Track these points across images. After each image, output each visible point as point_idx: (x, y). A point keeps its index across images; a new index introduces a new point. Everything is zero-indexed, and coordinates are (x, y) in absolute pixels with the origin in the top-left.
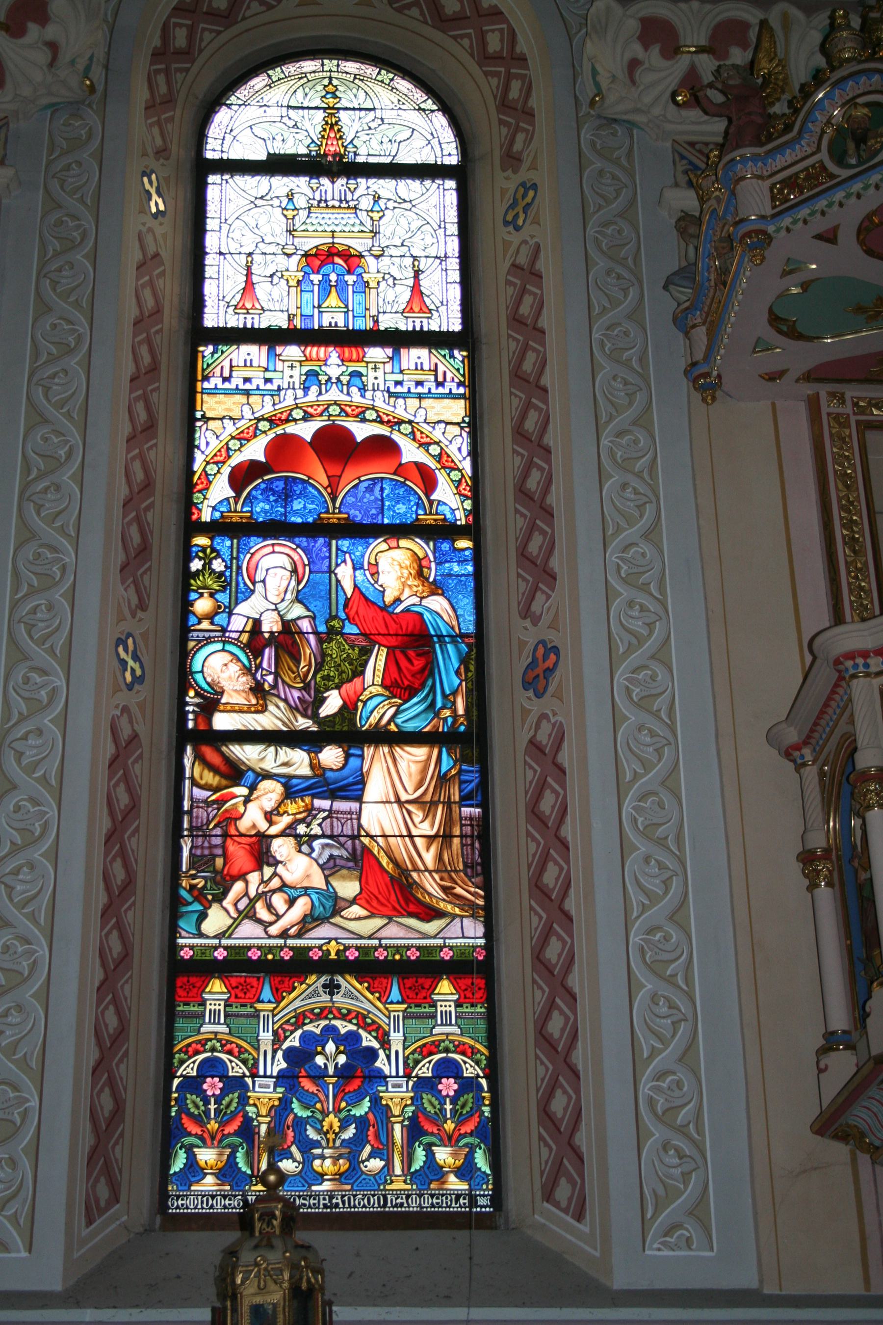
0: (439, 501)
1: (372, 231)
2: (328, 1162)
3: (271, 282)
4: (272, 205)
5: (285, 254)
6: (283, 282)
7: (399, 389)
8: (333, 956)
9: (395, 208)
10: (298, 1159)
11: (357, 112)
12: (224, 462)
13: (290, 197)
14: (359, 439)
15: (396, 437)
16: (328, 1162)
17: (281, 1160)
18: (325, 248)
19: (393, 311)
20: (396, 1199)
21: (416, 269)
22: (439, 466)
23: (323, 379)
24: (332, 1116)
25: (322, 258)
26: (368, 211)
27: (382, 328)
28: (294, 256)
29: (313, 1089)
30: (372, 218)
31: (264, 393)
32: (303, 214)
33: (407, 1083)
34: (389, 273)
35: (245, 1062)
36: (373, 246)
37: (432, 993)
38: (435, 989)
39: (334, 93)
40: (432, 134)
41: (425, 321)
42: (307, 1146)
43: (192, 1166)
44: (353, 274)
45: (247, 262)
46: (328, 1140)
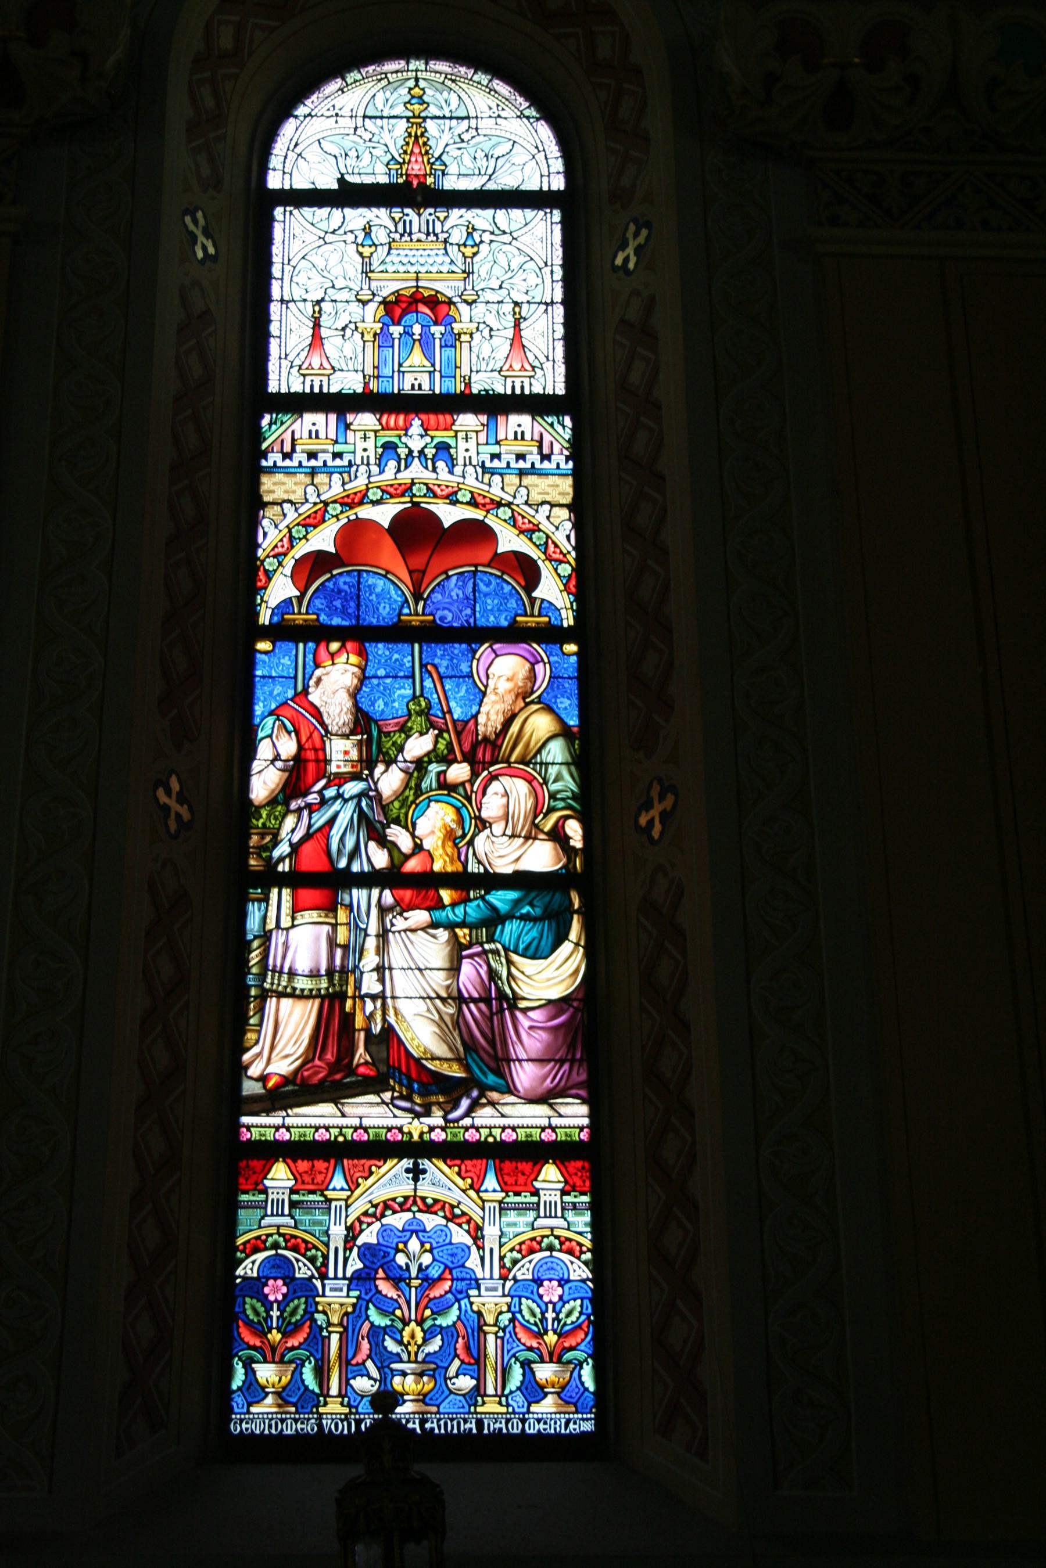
0: (543, 600)
1: (464, 272)
2: (410, 1379)
3: (343, 336)
4: (345, 241)
5: (359, 301)
6: (357, 336)
7: (496, 463)
8: (416, 1137)
9: (492, 241)
10: (375, 1376)
11: (447, 121)
12: (285, 554)
13: (367, 231)
14: (447, 524)
15: (491, 521)
16: (410, 1379)
17: (354, 1378)
18: (408, 293)
19: (489, 369)
20: (494, 1424)
21: (517, 316)
22: (543, 557)
23: (403, 452)
24: (413, 1324)
25: (404, 305)
26: (459, 245)
27: (475, 391)
28: (371, 304)
29: (392, 1293)
30: (463, 254)
31: (333, 470)
32: (382, 251)
33: (504, 1286)
34: (484, 323)
35: (312, 1260)
36: (465, 290)
37: (536, 1180)
38: (538, 1175)
39: (420, 97)
40: (537, 147)
41: (526, 381)
42: (384, 1361)
43: (251, 1384)
44: (441, 324)
45: (314, 312)
46: (409, 1353)
